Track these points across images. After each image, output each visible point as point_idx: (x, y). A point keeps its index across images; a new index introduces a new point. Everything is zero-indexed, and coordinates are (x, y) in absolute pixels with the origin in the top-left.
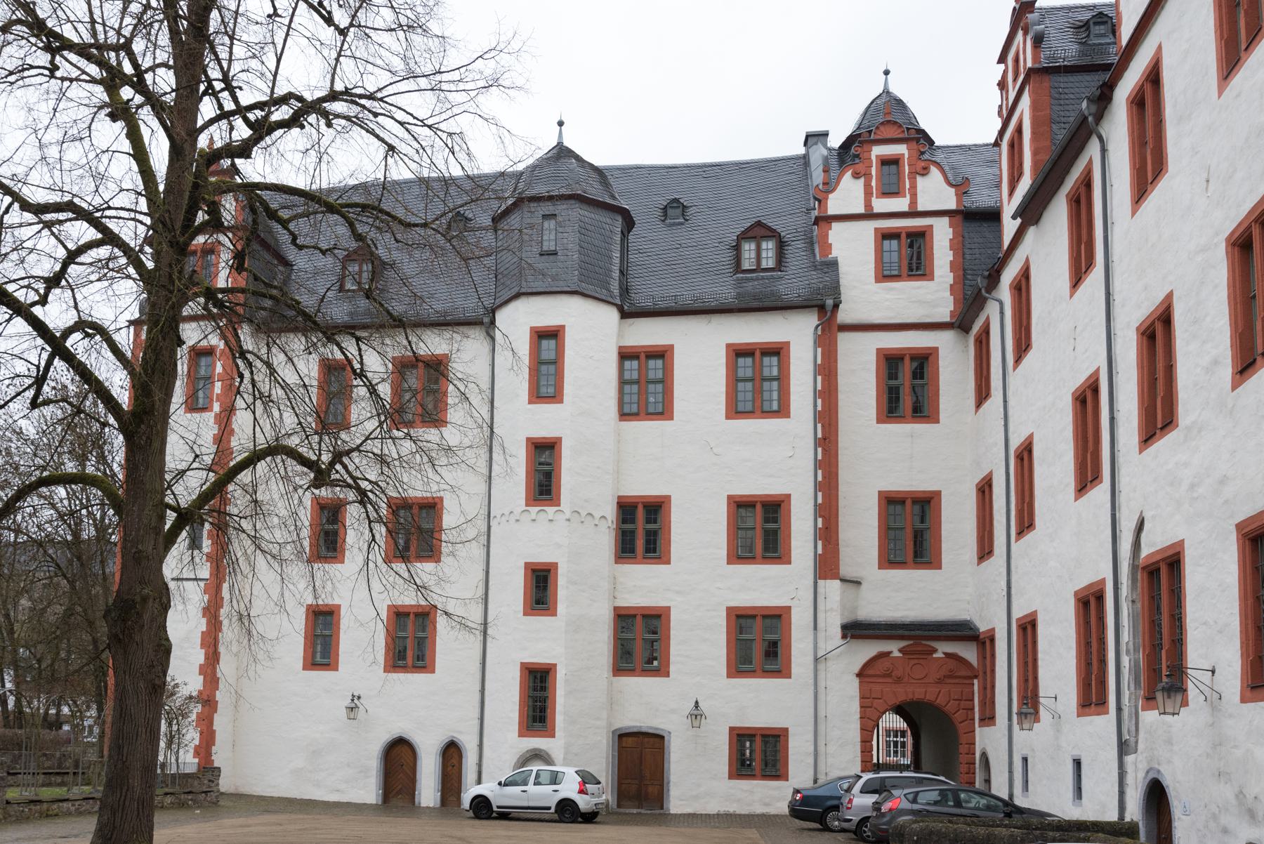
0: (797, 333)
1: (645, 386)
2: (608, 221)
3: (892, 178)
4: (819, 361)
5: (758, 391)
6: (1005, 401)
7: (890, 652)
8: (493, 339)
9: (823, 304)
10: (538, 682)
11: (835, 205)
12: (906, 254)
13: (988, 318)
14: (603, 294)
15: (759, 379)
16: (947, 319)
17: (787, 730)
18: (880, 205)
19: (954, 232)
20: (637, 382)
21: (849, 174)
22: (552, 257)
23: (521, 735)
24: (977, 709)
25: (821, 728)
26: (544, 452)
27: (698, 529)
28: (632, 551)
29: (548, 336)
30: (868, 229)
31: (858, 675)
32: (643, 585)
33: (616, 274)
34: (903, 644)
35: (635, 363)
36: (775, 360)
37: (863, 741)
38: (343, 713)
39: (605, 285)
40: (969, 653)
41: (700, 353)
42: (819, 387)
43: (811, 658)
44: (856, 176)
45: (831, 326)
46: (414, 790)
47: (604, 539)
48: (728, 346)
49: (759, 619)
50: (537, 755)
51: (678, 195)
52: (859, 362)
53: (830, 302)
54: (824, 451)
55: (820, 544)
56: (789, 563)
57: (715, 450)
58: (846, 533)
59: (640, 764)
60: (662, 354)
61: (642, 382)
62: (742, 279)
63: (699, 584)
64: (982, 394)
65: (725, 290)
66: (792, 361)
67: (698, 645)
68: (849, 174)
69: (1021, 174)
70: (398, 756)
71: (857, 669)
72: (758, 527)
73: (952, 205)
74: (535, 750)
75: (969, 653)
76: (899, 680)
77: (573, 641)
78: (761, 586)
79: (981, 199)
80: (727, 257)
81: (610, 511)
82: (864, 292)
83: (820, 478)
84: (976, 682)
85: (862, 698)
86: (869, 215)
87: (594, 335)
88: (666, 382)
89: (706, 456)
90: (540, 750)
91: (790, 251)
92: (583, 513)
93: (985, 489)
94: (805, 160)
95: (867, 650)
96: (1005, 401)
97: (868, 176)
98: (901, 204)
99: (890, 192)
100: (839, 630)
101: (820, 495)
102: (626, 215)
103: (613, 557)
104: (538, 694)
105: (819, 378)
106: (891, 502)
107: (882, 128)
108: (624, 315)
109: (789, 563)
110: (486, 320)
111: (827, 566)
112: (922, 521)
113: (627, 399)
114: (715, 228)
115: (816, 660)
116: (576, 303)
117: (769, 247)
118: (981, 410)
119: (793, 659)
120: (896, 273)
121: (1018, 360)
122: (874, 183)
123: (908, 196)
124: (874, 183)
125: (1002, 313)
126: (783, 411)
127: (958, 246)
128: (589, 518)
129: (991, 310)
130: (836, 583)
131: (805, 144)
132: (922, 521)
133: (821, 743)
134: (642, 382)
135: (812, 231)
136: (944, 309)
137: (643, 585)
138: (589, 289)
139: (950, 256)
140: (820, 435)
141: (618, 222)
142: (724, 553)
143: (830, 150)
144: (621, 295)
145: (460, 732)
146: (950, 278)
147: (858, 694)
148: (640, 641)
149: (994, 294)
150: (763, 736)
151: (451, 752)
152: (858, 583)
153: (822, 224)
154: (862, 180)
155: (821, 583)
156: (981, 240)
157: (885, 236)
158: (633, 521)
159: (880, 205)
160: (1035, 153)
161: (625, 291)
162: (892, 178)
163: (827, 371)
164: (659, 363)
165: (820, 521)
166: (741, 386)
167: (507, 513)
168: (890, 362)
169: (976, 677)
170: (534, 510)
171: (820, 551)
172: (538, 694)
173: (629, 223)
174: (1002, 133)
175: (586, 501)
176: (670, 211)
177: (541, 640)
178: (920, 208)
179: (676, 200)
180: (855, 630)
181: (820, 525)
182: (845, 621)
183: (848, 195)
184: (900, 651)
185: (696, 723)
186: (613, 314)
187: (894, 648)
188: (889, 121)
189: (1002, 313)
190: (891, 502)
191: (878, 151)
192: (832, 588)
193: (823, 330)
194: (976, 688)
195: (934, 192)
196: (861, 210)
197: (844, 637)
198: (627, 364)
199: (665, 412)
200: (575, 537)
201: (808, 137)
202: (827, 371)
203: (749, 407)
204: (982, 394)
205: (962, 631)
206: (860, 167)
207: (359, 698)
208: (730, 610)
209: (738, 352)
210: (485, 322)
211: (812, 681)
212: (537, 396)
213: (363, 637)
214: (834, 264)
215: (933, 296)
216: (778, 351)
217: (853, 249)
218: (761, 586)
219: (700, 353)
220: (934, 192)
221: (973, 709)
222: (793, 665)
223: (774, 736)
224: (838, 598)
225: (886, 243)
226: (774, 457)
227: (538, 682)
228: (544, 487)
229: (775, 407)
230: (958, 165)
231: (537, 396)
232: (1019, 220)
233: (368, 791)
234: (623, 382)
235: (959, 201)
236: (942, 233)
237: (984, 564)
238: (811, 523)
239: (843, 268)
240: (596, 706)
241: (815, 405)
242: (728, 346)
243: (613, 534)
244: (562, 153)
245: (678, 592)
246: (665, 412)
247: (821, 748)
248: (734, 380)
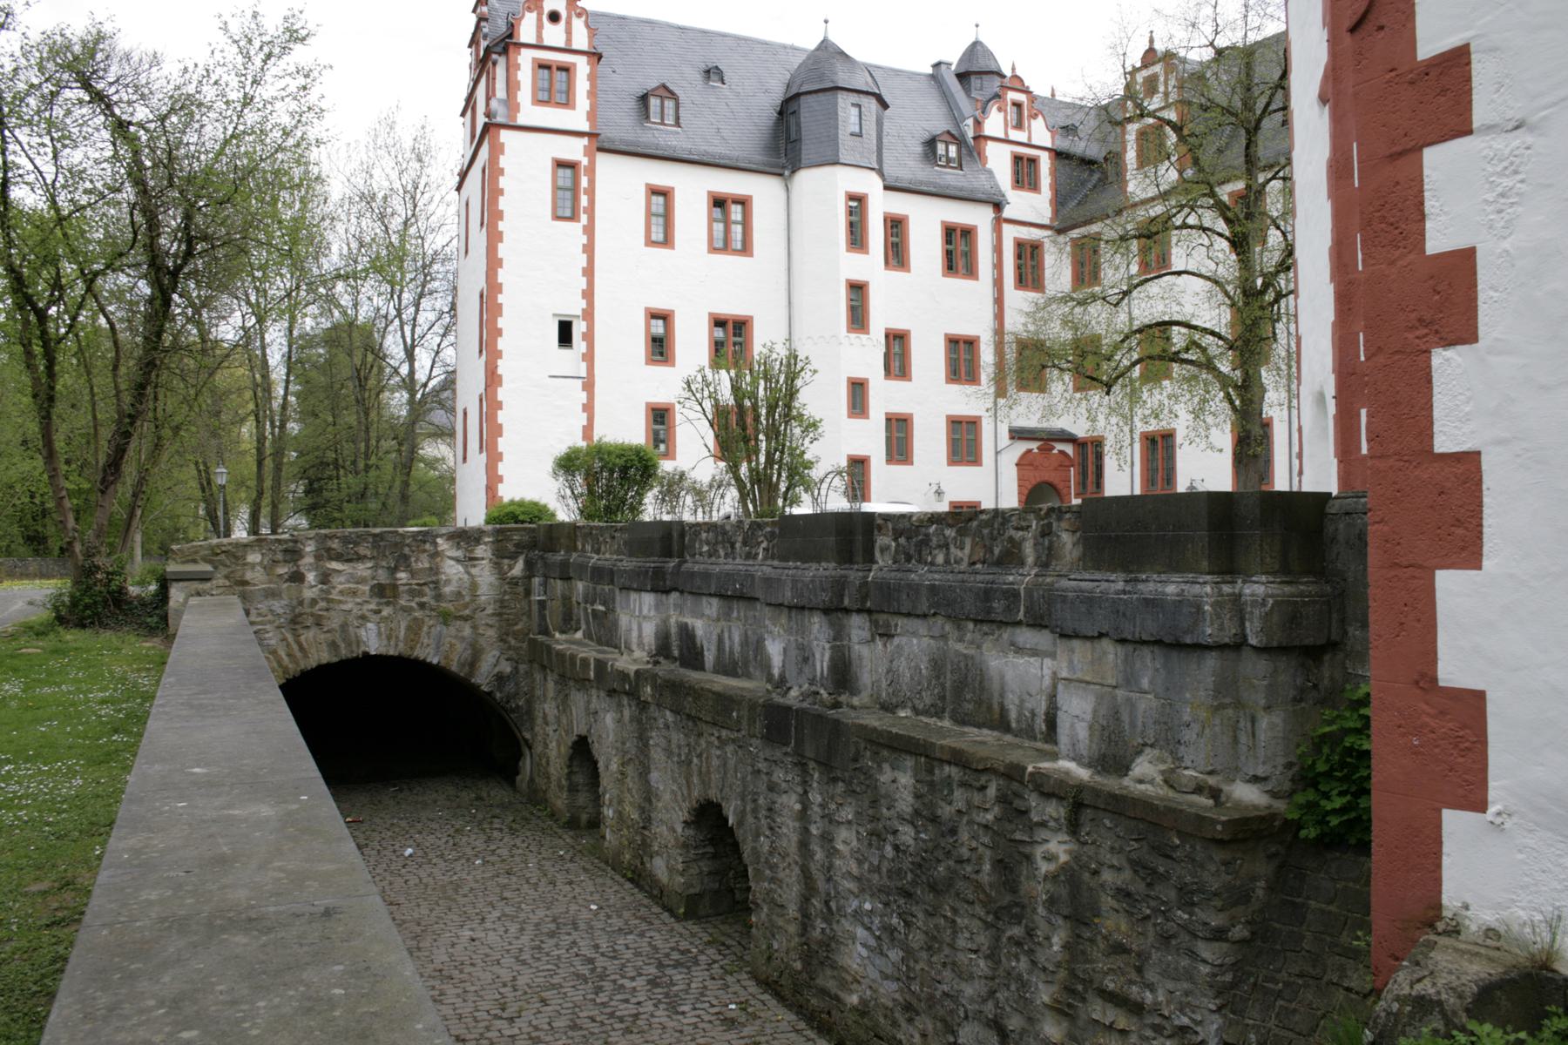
18: (1015, 135)
71: (1015, 460)
73: (1049, 145)
76: (1036, 468)
86: (1006, 141)
95: (1022, 447)
99: (1019, 126)
113: (560, 203)
115: (997, 453)
127: (1054, 172)
159: (1015, 135)
168: (1020, 245)
170: (853, 336)
178: (546, 43)
180: (1017, 434)
187: (1034, 446)
196: (562, 45)
208: (948, 417)
236: (1045, 162)
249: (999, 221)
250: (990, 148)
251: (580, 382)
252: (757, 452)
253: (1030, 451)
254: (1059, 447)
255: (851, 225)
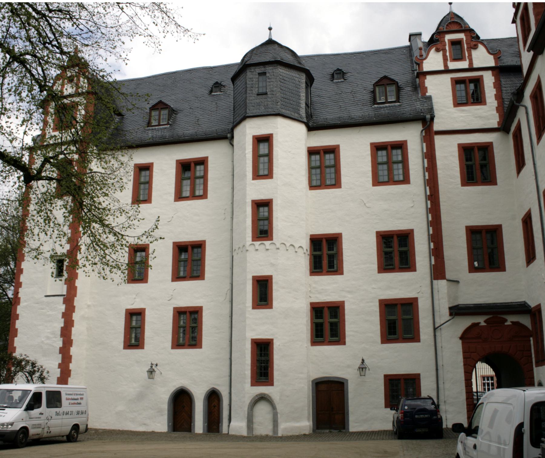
0: (411, 135)
1: (324, 169)
2: (297, 76)
3: (458, 51)
4: (425, 151)
5: (390, 171)
6: (534, 164)
7: (479, 323)
8: (233, 145)
9: (425, 120)
10: (263, 350)
11: (427, 66)
12: (469, 92)
13: (519, 121)
14: (296, 116)
15: (389, 163)
16: (496, 126)
17: (419, 375)
18: (452, 65)
19: (498, 103)
20: (319, 167)
21: (433, 50)
22: (264, 96)
23: (253, 384)
24: (533, 356)
25: (440, 372)
26: (263, 206)
27: (360, 253)
28: (321, 267)
29: (264, 140)
30: (447, 79)
31: (461, 338)
32: (327, 289)
33: (303, 105)
34: (486, 317)
35: (318, 157)
36: (399, 152)
37: (466, 380)
38: (146, 375)
39: (297, 111)
40: (526, 321)
41: (355, 149)
42: (426, 165)
43: (431, 329)
44: (438, 50)
45: (429, 135)
46: (191, 423)
47: (303, 261)
48: (372, 144)
49: (399, 306)
50: (262, 398)
51: (339, 68)
52: (447, 152)
53: (428, 117)
54: (431, 202)
55: (433, 258)
56: (415, 270)
57: (367, 205)
58: (447, 252)
59: (329, 401)
60: (333, 150)
61: (321, 167)
62: (378, 107)
63: (361, 287)
64: (520, 164)
65: (368, 112)
66: (409, 151)
67: (362, 323)
68: (433, 50)
69: (529, 30)
70: (181, 400)
71: (460, 333)
72: (394, 250)
73: (492, 64)
74: (261, 394)
75: (526, 321)
77: (287, 324)
78: (399, 285)
79: (509, 61)
80: (368, 97)
81: (306, 244)
82: (447, 113)
83: (430, 219)
84: (531, 339)
85: (464, 352)
87: (291, 140)
88: (336, 166)
89: (361, 208)
90: (265, 394)
91: (402, 93)
92: (288, 245)
93: (527, 221)
94: (409, 48)
95: (465, 323)
96: (534, 164)
97: (444, 51)
98: (464, 65)
99: (460, 58)
100: (448, 311)
101: (431, 229)
102: (308, 73)
103: (308, 272)
104: (263, 358)
105: (426, 160)
106: (473, 233)
107: (450, 26)
108: (310, 129)
109: (415, 270)
110: (229, 135)
111: (438, 271)
112: (492, 243)
114: (363, 82)
115: (435, 329)
116: (280, 121)
117: (391, 89)
118: (521, 174)
119: (421, 330)
120: (465, 102)
121: (539, 138)
122: (448, 54)
123: (468, 60)
124: (448, 54)
125: (527, 113)
126: (406, 180)
127: (498, 85)
128: (292, 247)
129: (521, 115)
130: (445, 281)
131: (410, 40)
132: (492, 243)
133: (441, 382)
134: (321, 167)
135: (416, 82)
136: (494, 121)
137: (327, 289)
138: (287, 113)
139: (494, 92)
140: (428, 193)
141: (303, 78)
142: (375, 266)
143: (424, 43)
144: (307, 117)
145: (218, 385)
146: (495, 104)
147: (461, 350)
148: (327, 323)
149: (522, 103)
150: (405, 379)
151: (213, 397)
152: (457, 282)
153: (422, 77)
154: (441, 52)
155: (435, 282)
156: (510, 83)
157: (456, 82)
158: (320, 250)
159: (452, 65)
160: (536, 15)
161: (309, 116)
162: (458, 51)
163: (430, 155)
164: (332, 156)
165: (432, 244)
166: (380, 167)
167: (241, 246)
169: (531, 336)
171: (433, 263)
172: (263, 358)
173: (310, 80)
174: (516, 14)
175: (289, 237)
176: (336, 76)
177: (258, 324)
178: (475, 65)
179: (338, 70)
180: (457, 311)
181: (432, 247)
182: (451, 305)
183: (433, 61)
184: (485, 322)
185: (363, 373)
186: (302, 128)
187: (481, 320)
188: (453, 22)
189: (527, 113)
190: (473, 233)
191: (448, 37)
192: (441, 284)
193: (426, 133)
194: (532, 342)
195: (482, 58)
196: (442, 68)
197: (451, 314)
198: (313, 157)
199: (337, 184)
200: (286, 261)
201: (411, 35)
202: (430, 155)
203: (386, 179)
204: (520, 164)
205: (521, 308)
206: (439, 46)
207: (157, 365)
209: (377, 148)
210: (226, 136)
211: (433, 343)
212: (257, 176)
213: (159, 328)
214: (430, 98)
215: (487, 114)
216: (401, 146)
217: (439, 89)
218: (399, 285)
219: (355, 149)
220: (482, 58)
221: (531, 356)
222: (421, 334)
223: (411, 379)
224: (446, 291)
225: (458, 86)
226: (402, 208)
227: (263, 350)
228: (263, 231)
229: (401, 178)
230: (494, 47)
231: (257, 176)
232: (532, 53)
233: (161, 424)
234: (311, 168)
235: (496, 62)
236: (489, 79)
237: (531, 265)
238: (426, 246)
239: (434, 100)
240: (300, 363)
241: (424, 176)
242: (372, 144)
243: (309, 257)
244: (270, 42)
245: (349, 292)
246: (337, 184)
247: (441, 386)
248: (375, 164)
249: (429, 135)
250: (429, 81)
251: (61, 299)
252: (419, 415)
253: (475, 326)
254: (510, 319)
255: (468, 173)
